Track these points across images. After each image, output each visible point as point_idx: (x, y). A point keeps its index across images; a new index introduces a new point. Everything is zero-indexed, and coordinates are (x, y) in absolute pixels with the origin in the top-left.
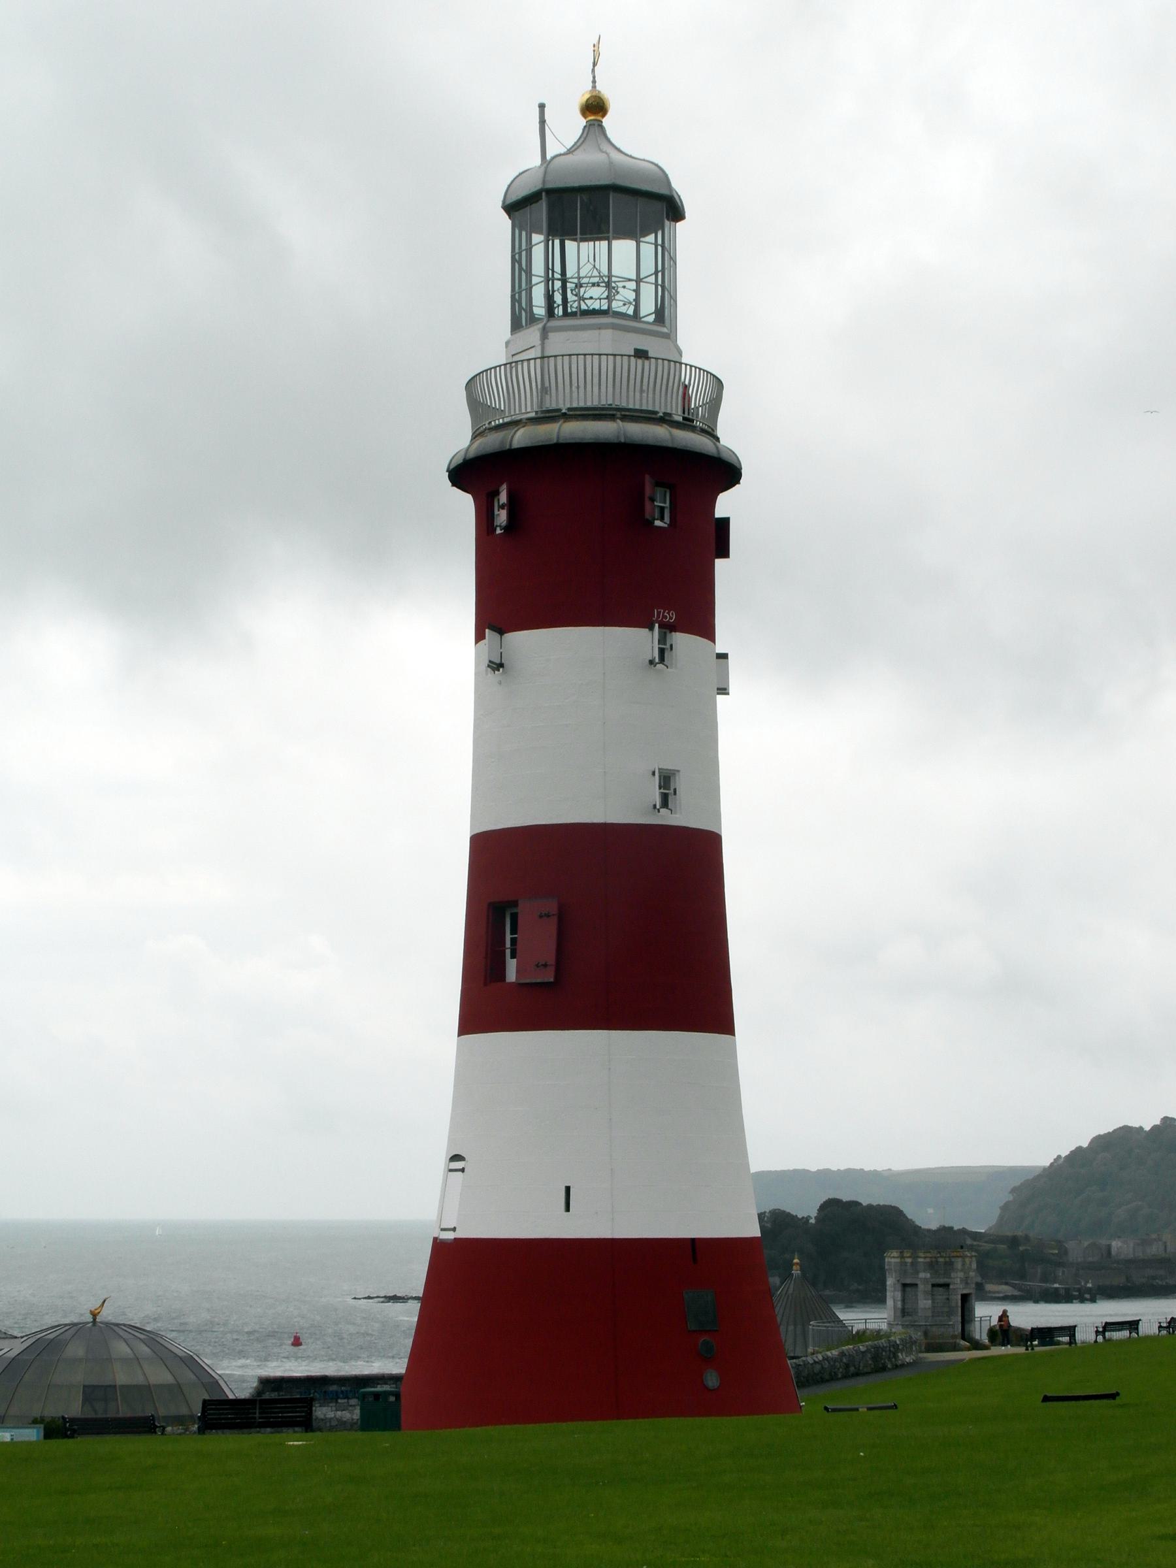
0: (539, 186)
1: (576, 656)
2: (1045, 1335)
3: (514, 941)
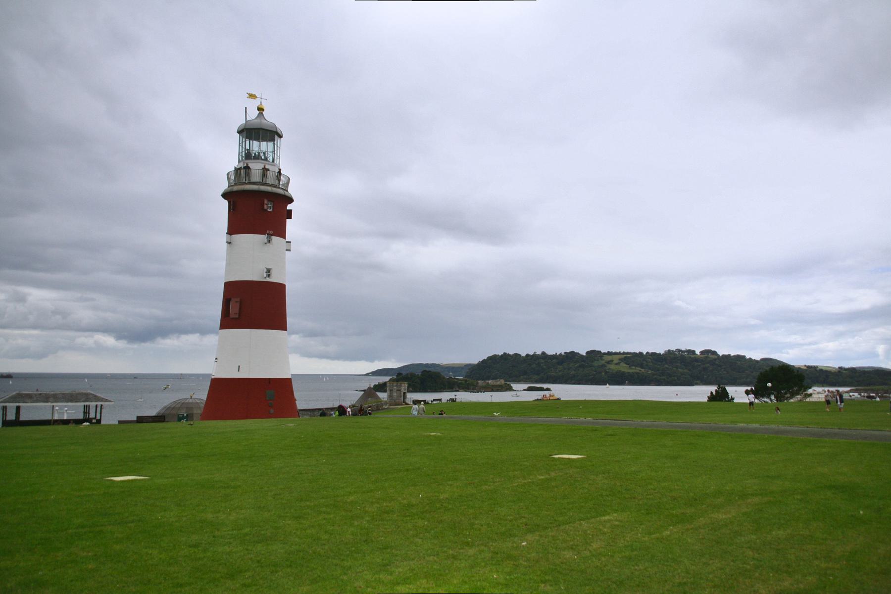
1: (250, 241)
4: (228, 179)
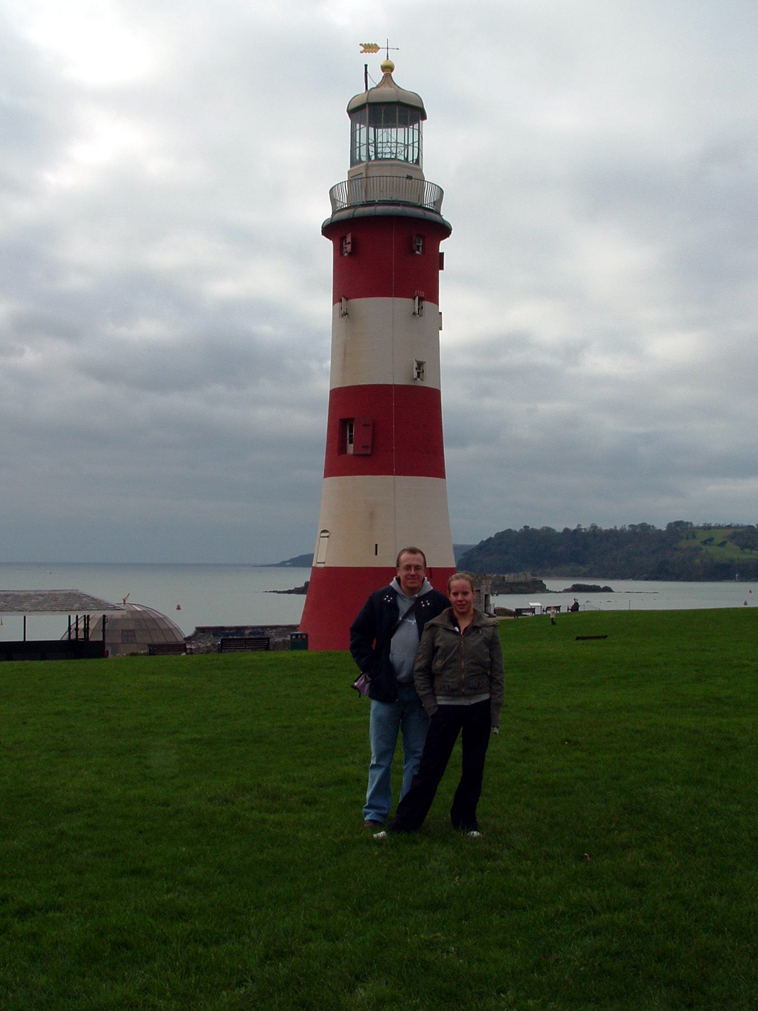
0: (365, 101)
1: (382, 311)
2: (519, 612)
3: (351, 436)
4: (333, 201)
